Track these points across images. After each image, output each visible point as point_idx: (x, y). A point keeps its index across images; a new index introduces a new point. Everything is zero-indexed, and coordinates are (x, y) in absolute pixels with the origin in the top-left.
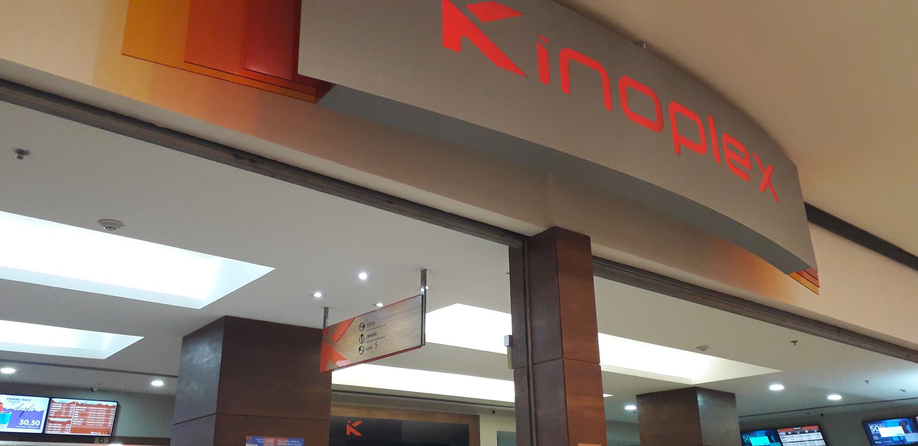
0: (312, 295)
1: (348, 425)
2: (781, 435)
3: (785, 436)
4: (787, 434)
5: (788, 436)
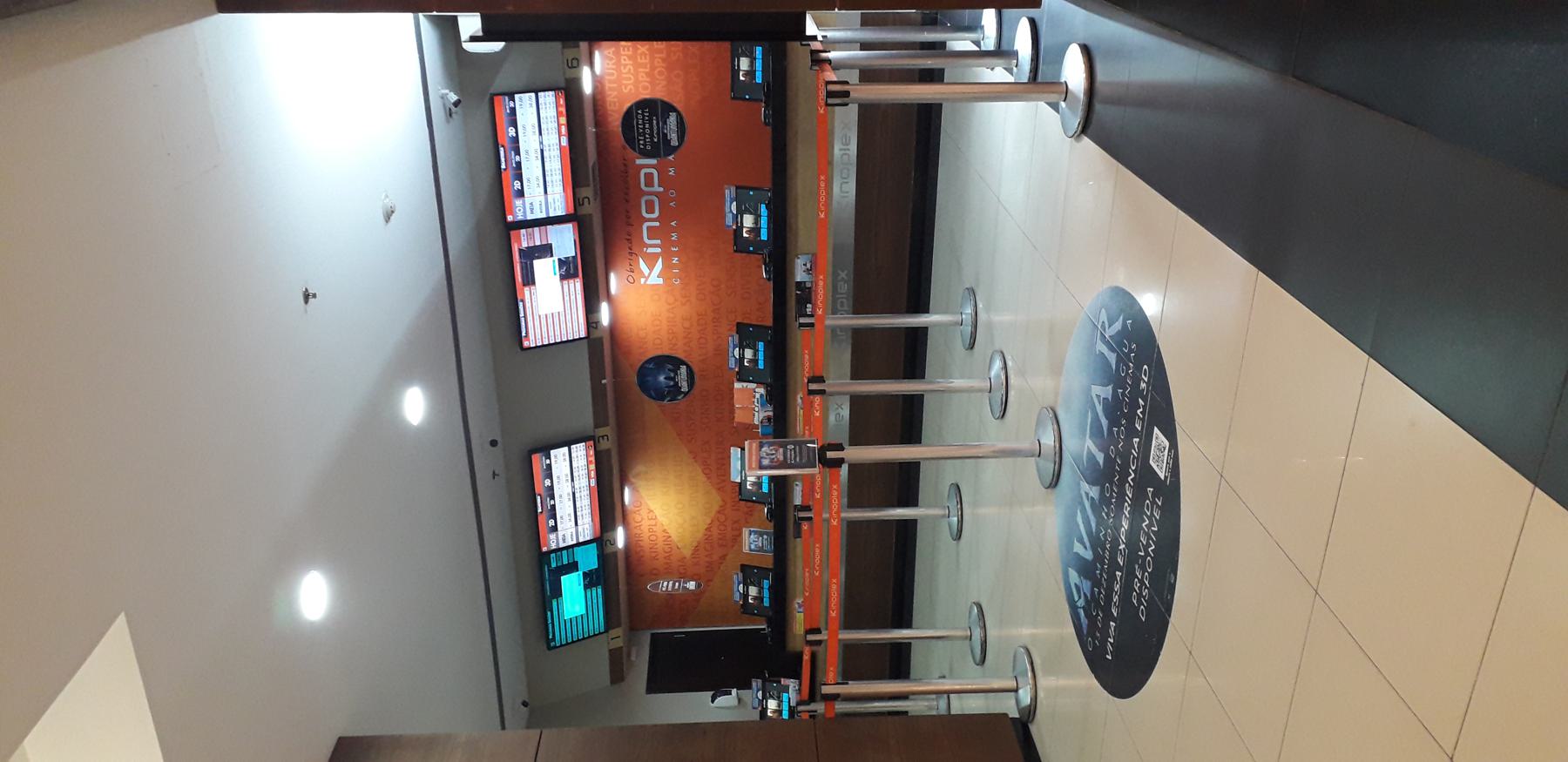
0: (1110, 621)
1: (648, 283)
2: (558, 543)
3: (560, 534)
4: (555, 529)
5: (559, 528)
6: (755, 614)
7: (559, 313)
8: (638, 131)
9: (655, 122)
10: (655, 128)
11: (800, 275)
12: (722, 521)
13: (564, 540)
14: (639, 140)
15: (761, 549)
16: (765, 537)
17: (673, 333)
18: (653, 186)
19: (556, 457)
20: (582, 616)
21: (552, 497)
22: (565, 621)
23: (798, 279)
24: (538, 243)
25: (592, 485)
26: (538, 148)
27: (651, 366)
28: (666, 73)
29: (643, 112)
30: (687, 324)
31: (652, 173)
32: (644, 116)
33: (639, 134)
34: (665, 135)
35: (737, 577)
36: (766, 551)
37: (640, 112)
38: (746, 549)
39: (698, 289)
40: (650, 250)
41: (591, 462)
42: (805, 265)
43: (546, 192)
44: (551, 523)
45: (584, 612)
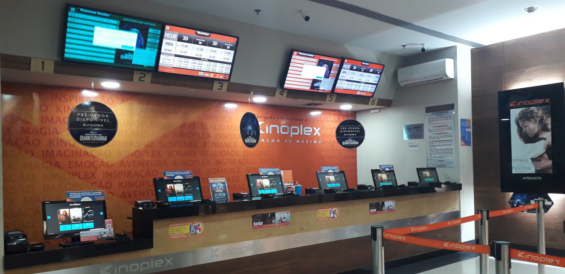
6: (200, 188)
7: (300, 75)
8: (349, 127)
9: (354, 135)
10: (350, 135)
11: (279, 215)
12: (95, 164)
13: (168, 44)
14: (357, 127)
15: (214, 192)
16: (224, 194)
17: (227, 136)
18: (293, 132)
19: (229, 53)
20: (92, 41)
21: (204, 44)
22: (94, 26)
23: (386, 203)
24: (149, 40)
25: (200, 73)
26: (203, 57)
27: (255, 122)
28: (330, 141)
29: (358, 130)
30: (232, 145)
31: (297, 132)
32: (357, 130)
33: (347, 127)
34: (347, 139)
35: (189, 174)
36: (213, 195)
37: (358, 128)
38: (211, 180)
39: (249, 151)
40: (267, 128)
41: (216, 76)
42: (284, 218)
43: (176, 56)
44: (186, 38)
45: (95, 43)
